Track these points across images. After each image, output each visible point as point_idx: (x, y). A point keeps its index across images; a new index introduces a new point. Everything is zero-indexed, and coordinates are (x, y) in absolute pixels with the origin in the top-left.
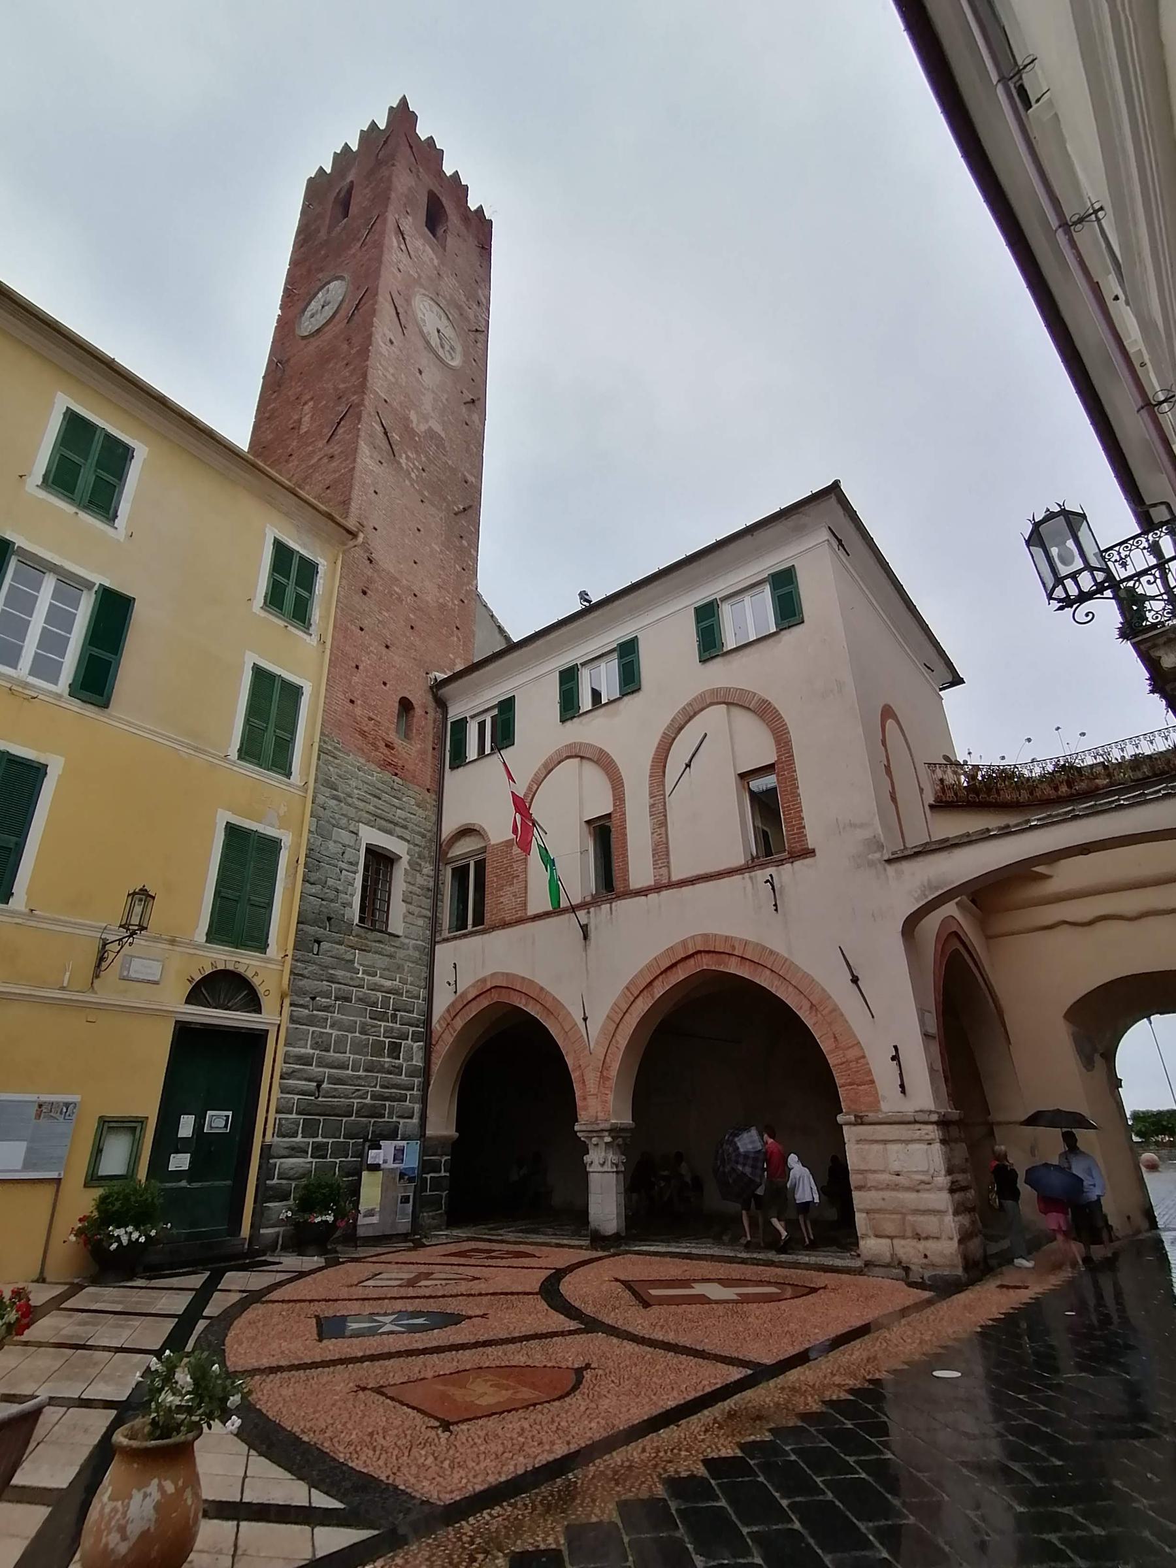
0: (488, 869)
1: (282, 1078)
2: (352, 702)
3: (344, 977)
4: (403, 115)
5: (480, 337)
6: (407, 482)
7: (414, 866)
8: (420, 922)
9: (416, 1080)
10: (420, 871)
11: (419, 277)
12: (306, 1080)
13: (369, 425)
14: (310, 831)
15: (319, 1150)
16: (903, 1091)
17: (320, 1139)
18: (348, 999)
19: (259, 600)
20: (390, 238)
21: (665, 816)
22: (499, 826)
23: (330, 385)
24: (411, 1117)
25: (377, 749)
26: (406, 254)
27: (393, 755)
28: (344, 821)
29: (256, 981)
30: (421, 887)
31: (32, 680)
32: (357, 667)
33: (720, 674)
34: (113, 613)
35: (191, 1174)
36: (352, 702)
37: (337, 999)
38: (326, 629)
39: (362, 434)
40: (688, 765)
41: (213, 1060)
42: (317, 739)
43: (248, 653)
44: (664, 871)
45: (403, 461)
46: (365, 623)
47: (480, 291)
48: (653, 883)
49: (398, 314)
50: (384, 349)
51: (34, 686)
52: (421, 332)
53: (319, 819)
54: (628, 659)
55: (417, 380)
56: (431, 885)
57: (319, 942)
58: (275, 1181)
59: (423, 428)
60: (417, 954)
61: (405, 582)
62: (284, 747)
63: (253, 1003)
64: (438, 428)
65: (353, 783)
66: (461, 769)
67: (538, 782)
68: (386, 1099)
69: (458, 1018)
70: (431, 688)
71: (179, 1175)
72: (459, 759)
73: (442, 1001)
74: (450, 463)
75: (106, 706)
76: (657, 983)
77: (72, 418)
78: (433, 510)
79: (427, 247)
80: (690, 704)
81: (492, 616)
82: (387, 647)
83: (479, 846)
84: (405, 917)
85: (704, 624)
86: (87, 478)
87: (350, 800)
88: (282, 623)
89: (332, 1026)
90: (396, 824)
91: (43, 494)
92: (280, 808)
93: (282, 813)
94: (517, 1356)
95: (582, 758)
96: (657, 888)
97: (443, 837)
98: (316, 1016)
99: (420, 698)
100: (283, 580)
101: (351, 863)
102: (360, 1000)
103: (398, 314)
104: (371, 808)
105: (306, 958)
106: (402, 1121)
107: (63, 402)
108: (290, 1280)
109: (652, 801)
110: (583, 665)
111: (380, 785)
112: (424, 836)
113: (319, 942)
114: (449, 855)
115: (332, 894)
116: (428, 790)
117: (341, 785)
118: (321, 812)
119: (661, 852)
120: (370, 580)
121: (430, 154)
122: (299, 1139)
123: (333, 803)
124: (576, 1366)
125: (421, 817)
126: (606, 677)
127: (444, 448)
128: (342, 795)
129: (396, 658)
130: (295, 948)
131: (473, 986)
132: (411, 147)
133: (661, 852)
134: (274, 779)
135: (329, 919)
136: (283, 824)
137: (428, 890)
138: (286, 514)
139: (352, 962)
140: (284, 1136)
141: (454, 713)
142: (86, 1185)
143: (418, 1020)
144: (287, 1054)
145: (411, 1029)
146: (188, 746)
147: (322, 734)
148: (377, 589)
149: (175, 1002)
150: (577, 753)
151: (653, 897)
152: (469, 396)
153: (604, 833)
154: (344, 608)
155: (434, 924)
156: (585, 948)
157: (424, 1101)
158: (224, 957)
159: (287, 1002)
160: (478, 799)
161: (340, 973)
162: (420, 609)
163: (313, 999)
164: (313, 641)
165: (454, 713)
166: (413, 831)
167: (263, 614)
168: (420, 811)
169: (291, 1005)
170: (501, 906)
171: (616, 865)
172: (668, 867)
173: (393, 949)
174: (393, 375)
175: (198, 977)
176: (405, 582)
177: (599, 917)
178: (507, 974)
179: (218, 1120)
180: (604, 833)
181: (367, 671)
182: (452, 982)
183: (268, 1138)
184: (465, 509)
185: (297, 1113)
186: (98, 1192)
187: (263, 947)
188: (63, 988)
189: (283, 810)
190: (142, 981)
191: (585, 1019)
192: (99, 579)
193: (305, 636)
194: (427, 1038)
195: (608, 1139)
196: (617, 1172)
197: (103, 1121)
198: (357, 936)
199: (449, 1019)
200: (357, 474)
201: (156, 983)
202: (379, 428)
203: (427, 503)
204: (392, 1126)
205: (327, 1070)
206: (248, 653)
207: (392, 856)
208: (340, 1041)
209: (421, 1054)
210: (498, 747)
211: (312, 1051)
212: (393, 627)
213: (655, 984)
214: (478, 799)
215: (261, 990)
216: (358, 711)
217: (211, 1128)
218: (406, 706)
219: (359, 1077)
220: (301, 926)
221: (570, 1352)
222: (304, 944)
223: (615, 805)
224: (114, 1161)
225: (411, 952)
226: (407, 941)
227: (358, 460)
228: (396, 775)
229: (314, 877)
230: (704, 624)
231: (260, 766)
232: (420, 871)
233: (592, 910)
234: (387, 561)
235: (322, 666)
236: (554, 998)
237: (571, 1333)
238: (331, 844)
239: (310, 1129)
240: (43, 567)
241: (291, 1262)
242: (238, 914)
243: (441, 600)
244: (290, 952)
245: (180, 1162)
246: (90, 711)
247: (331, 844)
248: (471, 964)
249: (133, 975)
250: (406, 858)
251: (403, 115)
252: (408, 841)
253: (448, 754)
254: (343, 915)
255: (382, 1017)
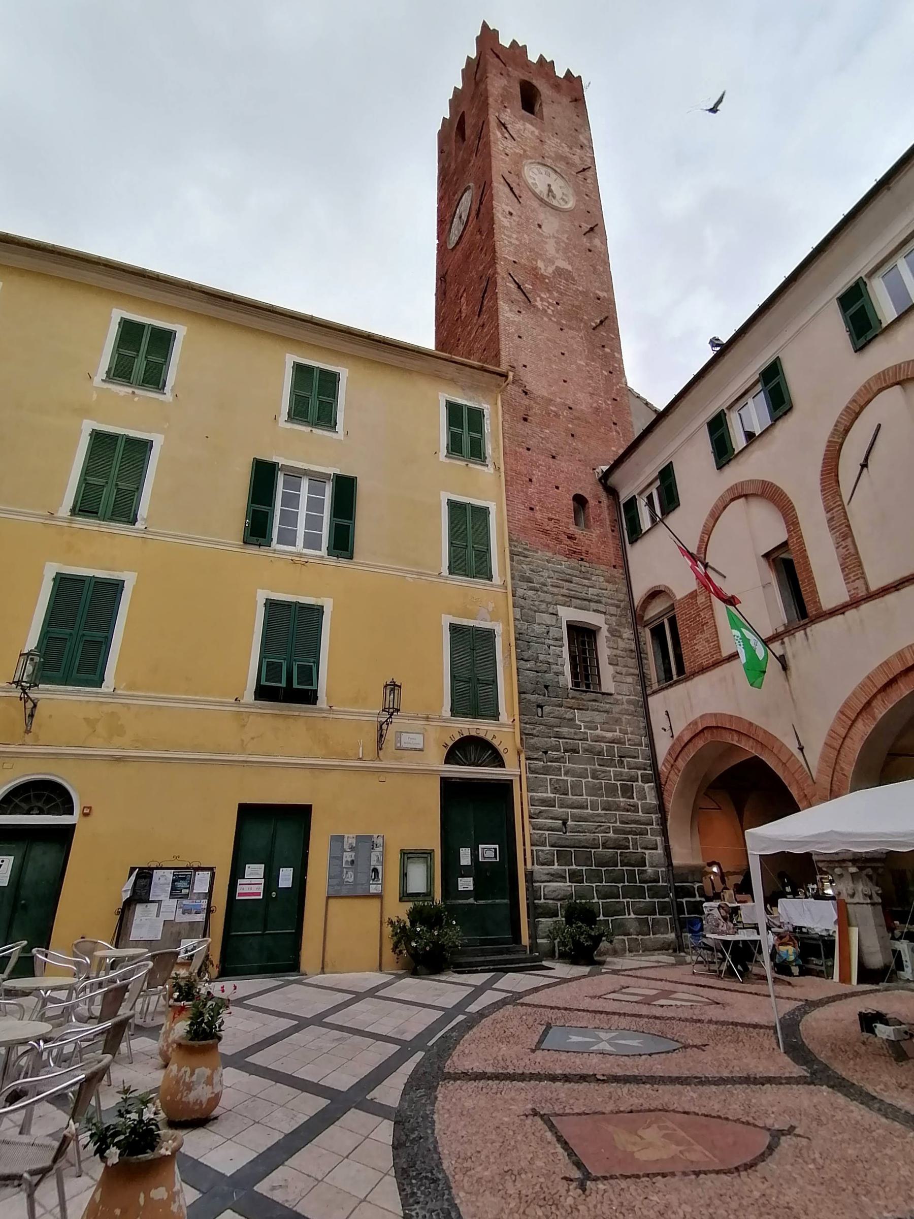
0: (679, 623)
1: (530, 817)
2: (531, 509)
3: (570, 733)
4: (487, 36)
5: (588, 173)
6: (545, 319)
7: (614, 633)
8: (630, 679)
9: (654, 816)
10: (620, 637)
11: (525, 151)
12: (552, 818)
13: (505, 286)
14: (515, 619)
15: (575, 877)
16: (880, 425)
17: (574, 867)
18: (575, 751)
19: (443, 451)
20: (495, 134)
21: (849, 526)
22: (682, 583)
23: (474, 273)
24: (656, 849)
25: (561, 542)
26: (512, 138)
27: (577, 544)
28: (544, 606)
29: (495, 742)
30: (625, 650)
31: (306, 551)
32: (530, 480)
33: (883, 355)
34: (345, 491)
35: (477, 893)
36: (531, 509)
37: (566, 751)
38: (498, 458)
39: (500, 296)
40: (864, 465)
41: (474, 805)
42: (507, 545)
43: (442, 493)
44: (859, 583)
45: (539, 304)
46: (531, 443)
47: (581, 137)
48: (848, 599)
49: (511, 189)
50: (505, 222)
51: (305, 555)
52: (534, 194)
53: (522, 608)
54: (772, 384)
55: (539, 234)
56: (633, 647)
57: (541, 707)
58: (543, 901)
59: (551, 270)
60: (632, 708)
61: (558, 400)
62: (483, 555)
63: (497, 760)
64: (563, 264)
65: (545, 574)
66: (639, 542)
67: (707, 532)
68: (630, 833)
69: (679, 759)
70: (600, 480)
71: (466, 894)
72: (636, 533)
73: (663, 746)
74: (581, 289)
75: (351, 558)
76: (876, 703)
77: (299, 369)
78: (572, 333)
79: (528, 126)
80: (854, 401)
81: (647, 404)
82: (554, 457)
83: (668, 604)
84: (614, 677)
85: (852, 310)
86: (313, 406)
87: (545, 588)
88: (463, 464)
89: (566, 774)
90: (590, 601)
91: (289, 426)
92: (488, 604)
93: (491, 610)
94: (712, 1100)
95: (746, 496)
96: (855, 603)
97: (636, 604)
98: (551, 766)
99: (590, 489)
100: (458, 430)
101: (556, 639)
102: (586, 750)
103: (511, 189)
104: (565, 591)
105: (533, 721)
106: (647, 852)
107: (291, 359)
108: (555, 984)
109: (829, 515)
110: (730, 408)
111: (569, 571)
112: (618, 607)
113: (541, 707)
114: (645, 619)
115: (544, 667)
116: (614, 567)
117: (536, 578)
118: (522, 602)
119: (852, 564)
120: (528, 408)
121: (518, 51)
122: (556, 867)
123: (531, 593)
124: (777, 1127)
125: (611, 591)
126: (755, 413)
127: (573, 279)
128: (538, 586)
129: (563, 464)
130: (521, 714)
131: (686, 729)
132: (498, 57)
133: (852, 564)
134: (479, 583)
135: (546, 687)
136: (494, 617)
137: (632, 651)
138: (452, 380)
139: (573, 720)
140: (543, 865)
141: (624, 497)
142: (401, 900)
143: (645, 764)
144: (532, 798)
145: (640, 772)
146: (412, 572)
147: (510, 540)
148: (535, 414)
149: (435, 761)
150: (740, 493)
151: (851, 613)
152: (586, 227)
153: (787, 566)
154: (510, 436)
155: (643, 678)
156: (787, 679)
157: (664, 833)
158: (467, 726)
159: (523, 757)
160: (658, 564)
161: (565, 730)
162: (578, 418)
163: (546, 753)
164: (491, 470)
165: (624, 497)
166: (606, 604)
167: (448, 461)
168: (610, 586)
169: (527, 759)
170: (697, 654)
171: (804, 588)
172: (864, 578)
173: (608, 706)
174: (517, 239)
175: (450, 744)
176: (558, 400)
177: (795, 646)
178: (715, 715)
179: (489, 852)
180: (787, 566)
181: (539, 481)
182: (667, 728)
183: (529, 866)
184: (601, 322)
185: (552, 846)
186: (410, 905)
187: (496, 716)
188: (360, 759)
189: (491, 606)
190: (411, 749)
191: (801, 749)
192: (332, 471)
193: (485, 469)
194: (656, 778)
195: (853, 870)
196: (873, 904)
197: (404, 853)
198: (573, 698)
199: (672, 761)
200: (501, 328)
201: (421, 750)
202: (512, 286)
203: (566, 330)
204: (639, 856)
205: (569, 810)
206: (442, 493)
207: (593, 628)
208: (576, 787)
209: (653, 793)
210: (666, 512)
211: (552, 795)
212: (555, 439)
213: (874, 704)
214: (658, 564)
215: (501, 749)
216: (538, 516)
217: (485, 858)
218: (580, 501)
219: (599, 815)
220: (523, 696)
221: (773, 1105)
222: (528, 710)
223: (789, 531)
224: (417, 882)
225: (625, 706)
226: (620, 697)
227: (501, 317)
228: (582, 560)
229: (525, 655)
230: (852, 310)
231: (467, 576)
232: (620, 637)
233: (786, 640)
234: (538, 386)
235: (500, 487)
236: (765, 732)
237: (790, 1081)
238: (536, 627)
239: (563, 858)
240: (295, 475)
241: (561, 969)
242: (472, 691)
243: (595, 405)
244: (517, 718)
245: (466, 884)
246: (343, 562)
247: (536, 627)
248: (681, 708)
249: (404, 746)
250: (605, 628)
251: (487, 36)
252: (605, 613)
253: (626, 532)
254: (558, 682)
255: (611, 763)
